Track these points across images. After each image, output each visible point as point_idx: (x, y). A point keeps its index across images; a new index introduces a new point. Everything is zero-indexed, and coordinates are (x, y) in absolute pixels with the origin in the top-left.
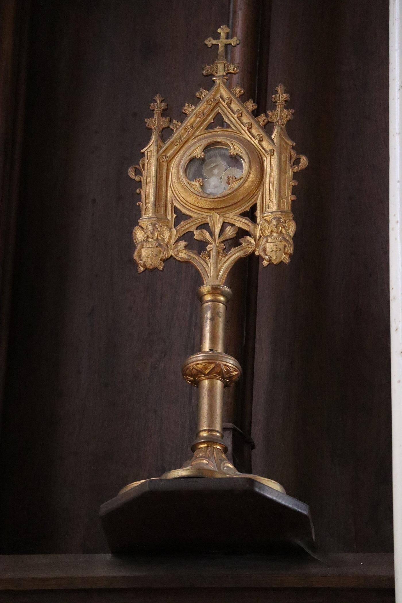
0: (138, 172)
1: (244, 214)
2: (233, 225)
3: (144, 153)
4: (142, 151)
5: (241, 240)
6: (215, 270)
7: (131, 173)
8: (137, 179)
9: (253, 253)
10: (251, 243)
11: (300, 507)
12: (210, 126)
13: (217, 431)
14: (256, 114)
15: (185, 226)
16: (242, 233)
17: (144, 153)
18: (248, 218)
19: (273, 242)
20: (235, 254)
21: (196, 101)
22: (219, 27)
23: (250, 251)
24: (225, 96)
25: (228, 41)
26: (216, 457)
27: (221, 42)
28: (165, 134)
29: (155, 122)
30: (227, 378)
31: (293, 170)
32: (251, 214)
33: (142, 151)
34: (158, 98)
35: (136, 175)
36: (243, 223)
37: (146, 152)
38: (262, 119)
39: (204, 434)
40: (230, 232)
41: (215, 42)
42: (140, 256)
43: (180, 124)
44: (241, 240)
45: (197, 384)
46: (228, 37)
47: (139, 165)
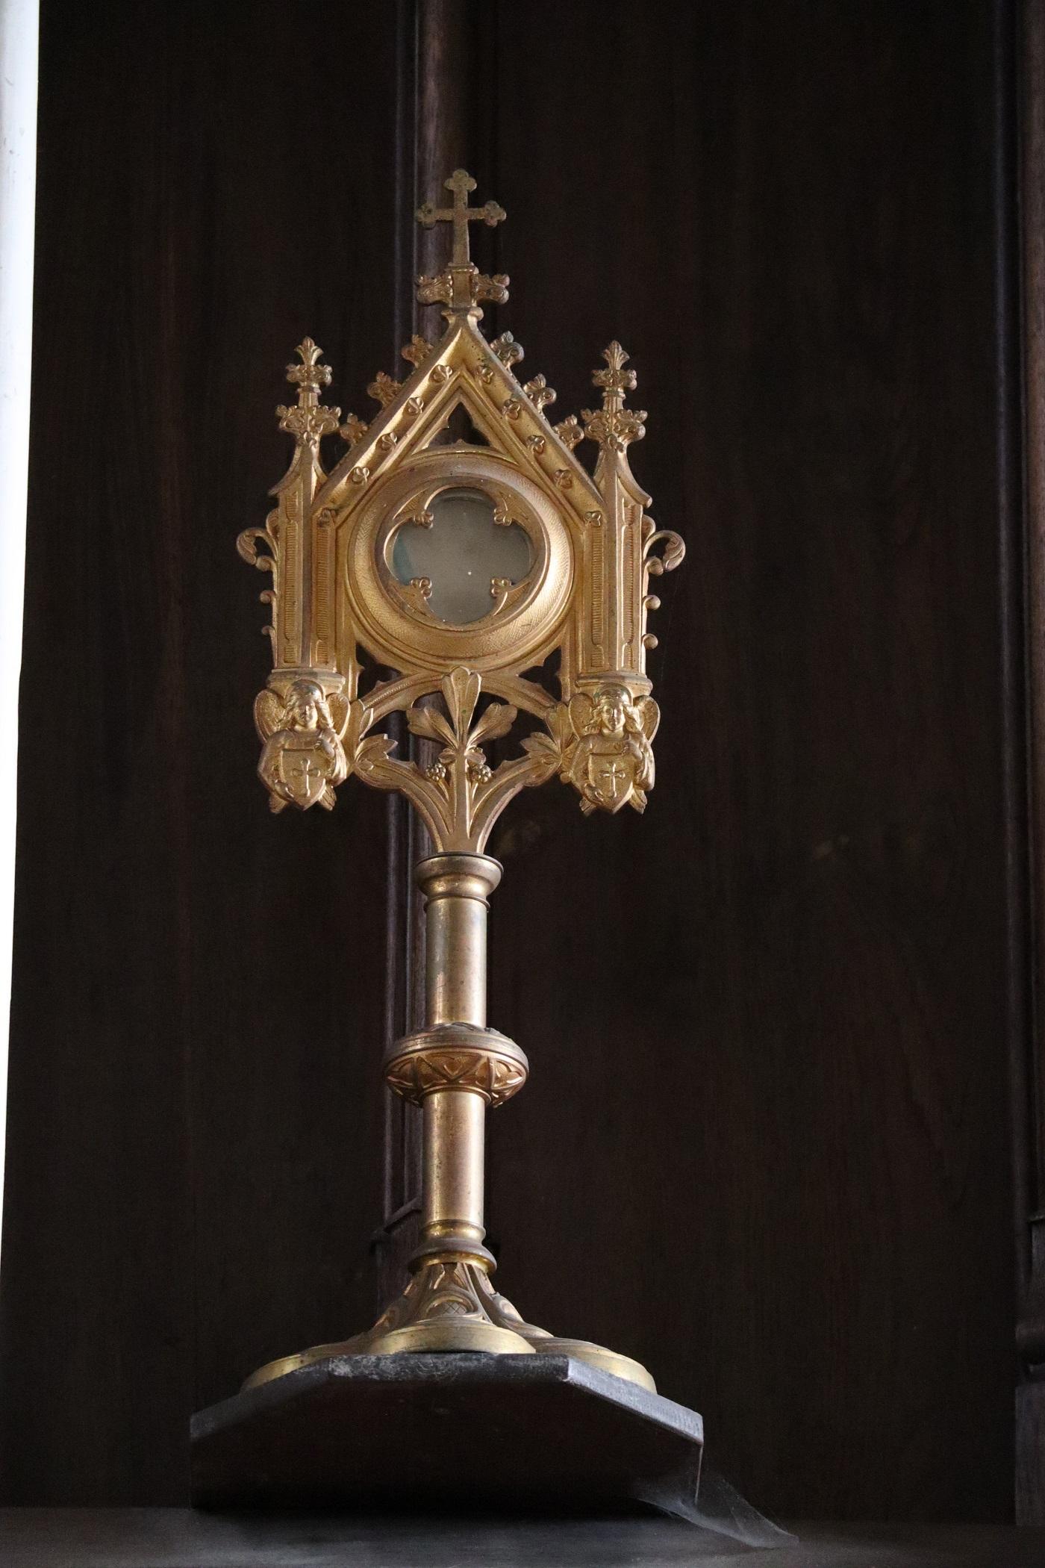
0: (263, 549)
2: (504, 702)
5: (527, 744)
6: (465, 808)
7: (244, 545)
8: (259, 563)
9: (556, 776)
11: (688, 1423)
13: (474, 1227)
15: (393, 698)
16: (527, 724)
18: (538, 686)
19: (618, 746)
20: (515, 778)
21: (523, 372)
23: (551, 769)
24: (460, 357)
25: (479, 214)
29: (308, 419)
30: (497, 1092)
31: (653, 564)
33: (273, 492)
34: (617, 357)
35: (258, 555)
39: (436, 1232)
40: (499, 720)
43: (365, 428)
44: (527, 744)
45: (422, 1100)
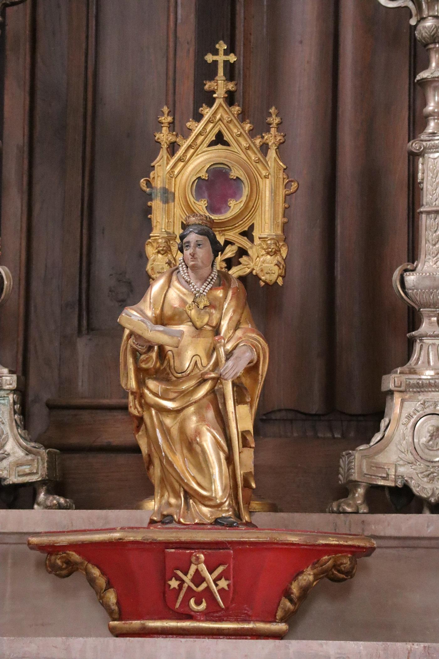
1: (244, 234)
3: (154, 166)
4: (152, 164)
10: (182, 333)
12: (212, 144)
14: (252, 134)
16: (242, 252)
17: (154, 166)
22: (217, 43)
26: (182, 512)
27: (221, 58)
28: (173, 148)
32: (248, 234)
36: (244, 242)
37: (156, 166)
38: (258, 141)
41: (221, 52)
42: (152, 269)
46: (226, 53)
47: (149, 178)
